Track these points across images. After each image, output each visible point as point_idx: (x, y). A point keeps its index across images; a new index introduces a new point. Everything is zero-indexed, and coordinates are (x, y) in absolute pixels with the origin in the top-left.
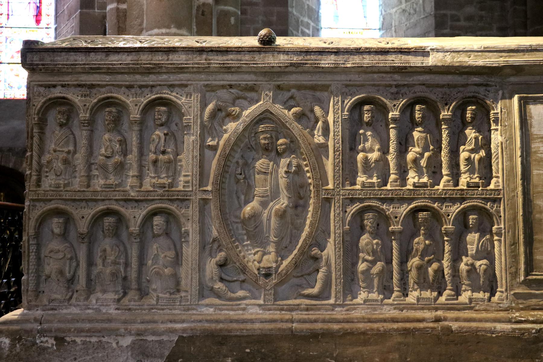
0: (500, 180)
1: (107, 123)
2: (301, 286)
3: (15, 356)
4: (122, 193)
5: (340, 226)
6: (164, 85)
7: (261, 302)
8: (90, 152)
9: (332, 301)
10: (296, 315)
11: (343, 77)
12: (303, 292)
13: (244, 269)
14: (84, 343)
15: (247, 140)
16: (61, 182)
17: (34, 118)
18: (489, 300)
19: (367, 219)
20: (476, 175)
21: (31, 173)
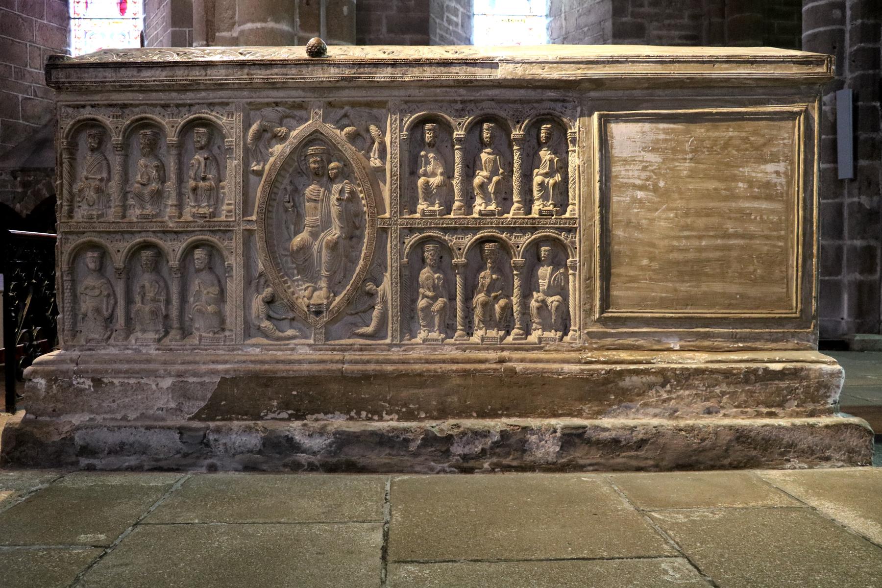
0: (577, 208)
1: (141, 146)
2: (356, 325)
3: (52, 397)
4: (160, 224)
5: (397, 259)
6: (203, 104)
7: (311, 341)
8: (125, 179)
9: (388, 341)
10: (348, 356)
11: (402, 92)
12: (357, 331)
13: (292, 306)
14: (122, 384)
15: (296, 164)
16: (94, 213)
17: (63, 143)
18: (561, 339)
19: (427, 251)
20: (550, 202)
21: (61, 203)
